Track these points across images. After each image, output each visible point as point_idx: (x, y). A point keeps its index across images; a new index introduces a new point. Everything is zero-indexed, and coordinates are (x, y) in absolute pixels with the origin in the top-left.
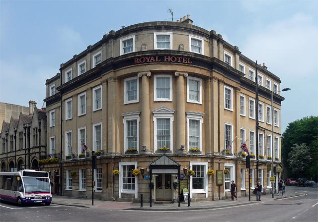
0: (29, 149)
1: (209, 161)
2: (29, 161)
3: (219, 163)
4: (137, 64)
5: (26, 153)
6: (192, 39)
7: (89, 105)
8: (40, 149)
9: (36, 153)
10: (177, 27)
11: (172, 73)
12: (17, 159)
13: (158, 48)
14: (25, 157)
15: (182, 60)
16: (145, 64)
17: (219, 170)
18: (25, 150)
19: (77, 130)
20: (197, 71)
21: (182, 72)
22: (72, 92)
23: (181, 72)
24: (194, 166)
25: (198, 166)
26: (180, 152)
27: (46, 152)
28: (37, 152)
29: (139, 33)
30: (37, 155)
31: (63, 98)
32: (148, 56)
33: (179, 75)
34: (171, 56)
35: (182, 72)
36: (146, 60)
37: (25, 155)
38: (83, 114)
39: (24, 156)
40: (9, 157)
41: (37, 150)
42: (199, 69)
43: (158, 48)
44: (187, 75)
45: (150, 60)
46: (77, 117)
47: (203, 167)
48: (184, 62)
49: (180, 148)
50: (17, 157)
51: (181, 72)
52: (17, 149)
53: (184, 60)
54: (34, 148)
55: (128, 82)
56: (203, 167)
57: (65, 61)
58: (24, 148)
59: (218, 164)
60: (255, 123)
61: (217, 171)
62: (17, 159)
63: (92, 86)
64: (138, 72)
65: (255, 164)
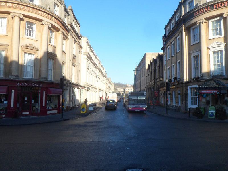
0: (156, 79)
4: (196, 16)
9: (158, 81)
11: (221, 16)
15: (221, 5)
16: (201, 14)
18: (155, 80)
28: (159, 81)
32: (202, 8)
34: (219, 3)
36: (201, 12)
45: (204, 11)
50: (152, 84)
54: (158, 78)
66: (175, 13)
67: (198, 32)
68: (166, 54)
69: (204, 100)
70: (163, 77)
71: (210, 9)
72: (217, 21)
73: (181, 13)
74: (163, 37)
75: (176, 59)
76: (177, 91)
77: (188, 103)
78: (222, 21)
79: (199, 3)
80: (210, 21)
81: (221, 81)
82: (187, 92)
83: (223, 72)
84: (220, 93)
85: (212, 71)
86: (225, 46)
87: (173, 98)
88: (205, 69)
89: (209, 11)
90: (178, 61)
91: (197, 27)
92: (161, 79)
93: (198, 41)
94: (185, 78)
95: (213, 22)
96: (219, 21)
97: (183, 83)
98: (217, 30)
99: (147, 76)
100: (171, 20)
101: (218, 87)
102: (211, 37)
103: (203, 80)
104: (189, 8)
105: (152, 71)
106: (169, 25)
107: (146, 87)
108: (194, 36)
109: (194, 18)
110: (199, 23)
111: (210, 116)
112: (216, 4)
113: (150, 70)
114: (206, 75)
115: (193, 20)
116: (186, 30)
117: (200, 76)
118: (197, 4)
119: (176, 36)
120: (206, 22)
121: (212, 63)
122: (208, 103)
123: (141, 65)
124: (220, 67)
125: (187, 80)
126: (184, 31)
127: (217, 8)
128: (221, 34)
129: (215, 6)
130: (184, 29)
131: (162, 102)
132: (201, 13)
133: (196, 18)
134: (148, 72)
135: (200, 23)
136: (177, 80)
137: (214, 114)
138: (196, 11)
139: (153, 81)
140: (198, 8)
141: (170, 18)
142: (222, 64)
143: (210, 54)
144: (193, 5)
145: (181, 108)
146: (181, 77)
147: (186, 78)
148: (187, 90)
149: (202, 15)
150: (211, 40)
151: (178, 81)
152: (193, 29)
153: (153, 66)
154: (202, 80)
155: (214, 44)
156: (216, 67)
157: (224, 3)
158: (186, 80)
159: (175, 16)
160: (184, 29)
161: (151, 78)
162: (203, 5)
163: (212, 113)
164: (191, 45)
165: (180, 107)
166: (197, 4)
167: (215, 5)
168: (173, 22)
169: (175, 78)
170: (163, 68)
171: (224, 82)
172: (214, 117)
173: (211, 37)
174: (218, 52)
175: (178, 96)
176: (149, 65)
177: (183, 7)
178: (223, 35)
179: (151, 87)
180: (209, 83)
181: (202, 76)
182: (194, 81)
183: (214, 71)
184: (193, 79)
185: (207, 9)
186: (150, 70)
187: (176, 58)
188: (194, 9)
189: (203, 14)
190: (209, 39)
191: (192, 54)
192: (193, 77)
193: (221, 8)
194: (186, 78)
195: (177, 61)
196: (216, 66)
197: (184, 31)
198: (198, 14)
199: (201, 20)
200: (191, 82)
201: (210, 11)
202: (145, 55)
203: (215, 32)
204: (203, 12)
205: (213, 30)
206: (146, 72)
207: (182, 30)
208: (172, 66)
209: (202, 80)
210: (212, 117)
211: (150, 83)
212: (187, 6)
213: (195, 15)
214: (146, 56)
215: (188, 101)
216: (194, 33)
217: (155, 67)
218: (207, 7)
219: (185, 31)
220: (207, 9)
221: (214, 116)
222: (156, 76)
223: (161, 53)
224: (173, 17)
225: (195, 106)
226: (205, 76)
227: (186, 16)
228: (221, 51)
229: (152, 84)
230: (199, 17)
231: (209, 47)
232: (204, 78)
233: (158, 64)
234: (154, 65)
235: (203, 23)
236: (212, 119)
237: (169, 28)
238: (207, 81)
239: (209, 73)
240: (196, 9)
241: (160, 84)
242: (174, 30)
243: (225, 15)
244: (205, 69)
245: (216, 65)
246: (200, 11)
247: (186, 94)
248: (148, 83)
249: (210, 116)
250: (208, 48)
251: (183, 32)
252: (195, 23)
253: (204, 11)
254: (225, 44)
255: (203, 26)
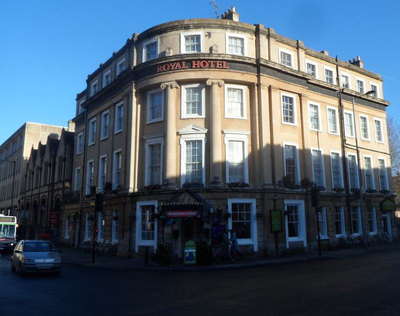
0: (53, 184)
1: (259, 197)
2: (52, 201)
3: (274, 201)
4: (161, 72)
5: (50, 189)
6: (231, 38)
7: (111, 126)
8: (64, 184)
9: (58, 189)
10: (209, 24)
11: (202, 82)
12: (41, 197)
13: (187, 51)
14: (48, 195)
15: (205, 64)
16: (169, 72)
17: (275, 209)
19: (99, 158)
20: (238, 76)
21: (216, 79)
22: (97, 109)
23: (214, 79)
24: (234, 205)
25: (241, 205)
26: (214, 185)
27: (71, 188)
28: (61, 189)
29: (164, 35)
30: (60, 192)
31: (89, 118)
32: (173, 62)
33: (213, 83)
34: (201, 60)
35: (216, 79)
36: (171, 67)
37: (48, 192)
38: (106, 137)
39: (47, 194)
40: (34, 195)
41: (61, 186)
42: (240, 74)
43: (187, 51)
44: (223, 82)
45: (175, 67)
46: (99, 141)
47: (248, 206)
48: (218, 67)
49: (212, 180)
50: (41, 195)
51: (214, 79)
52: (42, 185)
53: (218, 64)
54: (59, 182)
55: (152, 95)
56: (248, 206)
57: (91, 72)
58: (48, 183)
59: (272, 202)
60: (340, 139)
61: (270, 211)
62: (41, 197)
63: (115, 102)
64: (208, 79)
65: (344, 199)
66: (116, 56)
67: (160, 101)
68: (86, 131)
69: (168, 230)
70: (70, 181)
71: (186, 66)
72: (195, 90)
73: (130, 60)
74: (79, 97)
75: (113, 147)
76: (110, 212)
77: (135, 237)
78: (203, 91)
79: (167, 51)
80: (183, 87)
81: (199, 194)
82: (136, 214)
83: (202, 179)
84: (201, 215)
85: (183, 175)
86: (206, 134)
87: (111, 228)
88: (172, 172)
89: (183, 70)
90: (116, 151)
91: (161, 92)
92: (67, 185)
93: (161, 119)
94: (131, 185)
95: (188, 89)
96: (198, 90)
97: (127, 195)
98: (194, 104)
99: (26, 176)
100: (103, 68)
101: (199, 206)
102: (184, 115)
103: (168, 191)
104: (148, 55)
105: (35, 168)
106: (99, 76)
107: (19, 201)
108: (153, 108)
109: (156, 75)
110: (165, 87)
111: (188, 259)
112: (196, 60)
113: (38, 162)
114: (174, 182)
115: (154, 79)
116: (138, 94)
117: (161, 184)
118: (164, 53)
119: (114, 100)
120: (177, 88)
121: (184, 161)
122: (175, 234)
123: (7, 148)
124: (197, 170)
125: (136, 190)
126: (134, 94)
127: (198, 68)
128: (200, 113)
129: (195, 64)
130: (134, 91)
131: (67, 237)
132: (170, 70)
133: (161, 76)
134: (31, 166)
135: (167, 86)
136: (111, 189)
137: (194, 255)
138: (162, 64)
139: (46, 189)
140: (166, 60)
141: (103, 62)
142: (200, 164)
143: (181, 145)
144: (156, 52)
145: (120, 248)
146: (123, 183)
147: (133, 186)
148: (135, 209)
149: (172, 75)
150: (183, 121)
151: (116, 192)
152: (152, 95)
153: (47, 157)
154: (166, 191)
155: (189, 129)
156: (190, 169)
157: (209, 62)
158: (134, 190)
159: (113, 62)
160: (134, 91)
161: (30, 183)
162: (175, 56)
163: (191, 253)
164: (148, 123)
165: (116, 245)
166: (164, 53)
167: (194, 62)
168: (108, 72)
169: (108, 186)
170: (73, 161)
171: (203, 196)
172: (194, 262)
173: (184, 115)
174: (194, 142)
175: (111, 223)
176: (34, 152)
177: (135, 50)
178: (203, 116)
179: (28, 203)
180: (182, 196)
181: (166, 183)
182: (151, 194)
183: (187, 176)
184: (148, 188)
185: (181, 66)
186: (38, 162)
187: (113, 144)
188: (154, 61)
189: (173, 71)
190: (180, 119)
191: (147, 141)
192: (146, 184)
193: (204, 69)
194: (133, 186)
195: (113, 150)
196: (191, 167)
197: (134, 94)
198: (164, 69)
199: (169, 83)
200: (144, 195)
201: (185, 70)
202: (23, 128)
203: (191, 107)
204: (173, 68)
205: (188, 103)
206: (24, 166)
207: (131, 92)
208: (100, 160)
209: (166, 191)
210: (191, 261)
211: (36, 191)
212: (144, 51)
213: (158, 72)
214: (26, 130)
215: (135, 232)
216: (153, 102)
217: (54, 156)
218: (180, 62)
219: (136, 96)
220: (181, 66)
221: (194, 259)
222: (53, 177)
223: (72, 128)
224: (109, 63)
225: (153, 243)
226: (172, 184)
227: (142, 68)
228: (200, 142)
229: (41, 195)
230: (166, 75)
231: (181, 132)
232: (169, 187)
233: (61, 151)
234: (50, 152)
235: (172, 88)
236: (193, 265)
237: (97, 81)
238: (177, 193)
239: (178, 179)
240: (161, 61)
241: (64, 196)
242: (111, 89)
243: (209, 83)
244: (172, 172)
245: (190, 164)
246: (169, 66)
247: (133, 218)
248: (28, 191)
249: (188, 259)
250: (178, 134)
251: (132, 96)
252: (158, 85)
253: (176, 68)
254: (206, 131)
255: (172, 94)
